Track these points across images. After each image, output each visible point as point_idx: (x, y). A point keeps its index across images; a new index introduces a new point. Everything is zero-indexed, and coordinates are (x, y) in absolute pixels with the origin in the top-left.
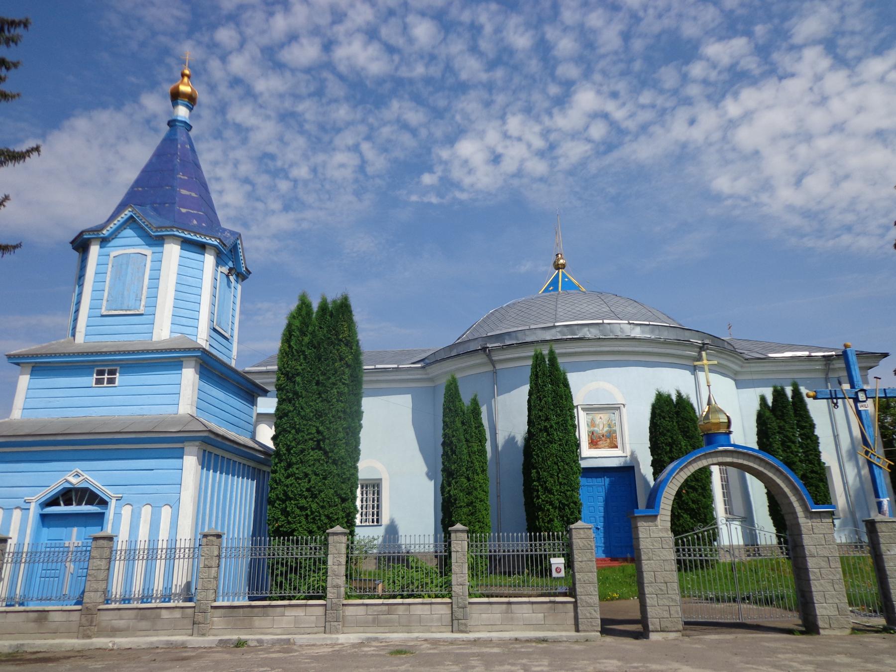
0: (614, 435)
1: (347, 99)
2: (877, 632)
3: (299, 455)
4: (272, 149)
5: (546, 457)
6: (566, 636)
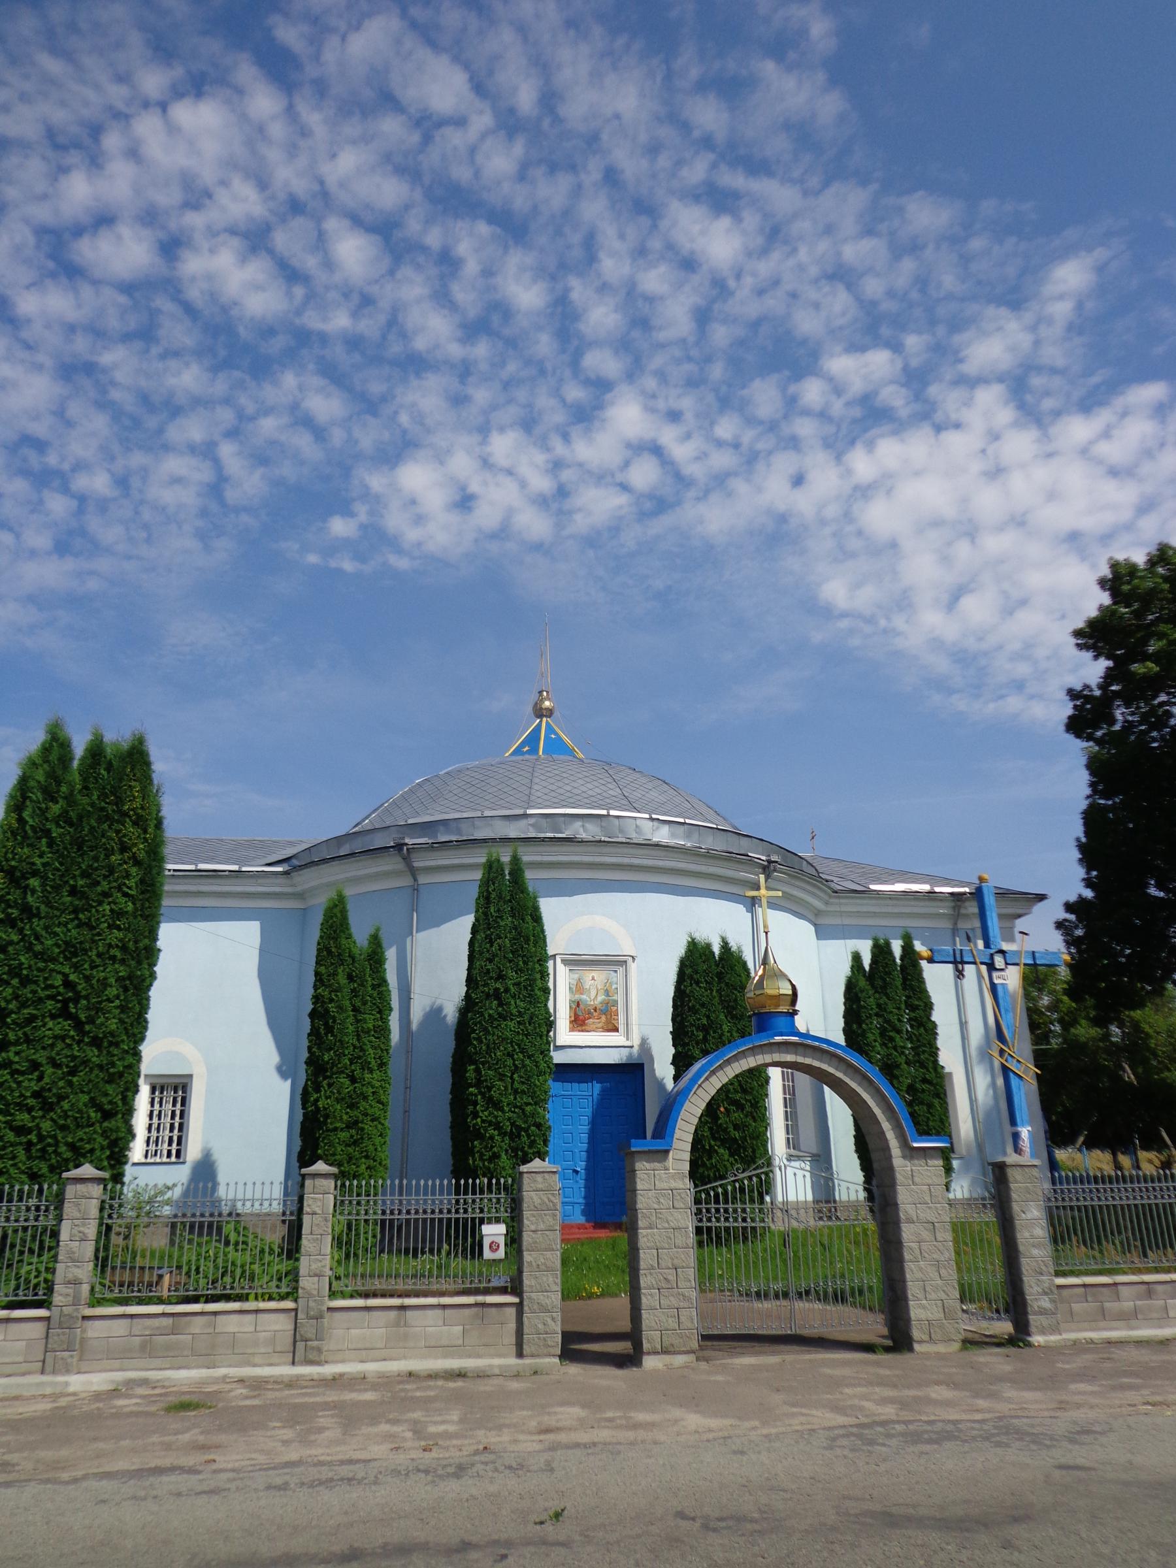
0: (614, 1009)
1: (199, 353)
2: (999, 1345)
3: (24, 1027)
4: (39, 429)
5: (494, 1043)
6: (500, 1367)
